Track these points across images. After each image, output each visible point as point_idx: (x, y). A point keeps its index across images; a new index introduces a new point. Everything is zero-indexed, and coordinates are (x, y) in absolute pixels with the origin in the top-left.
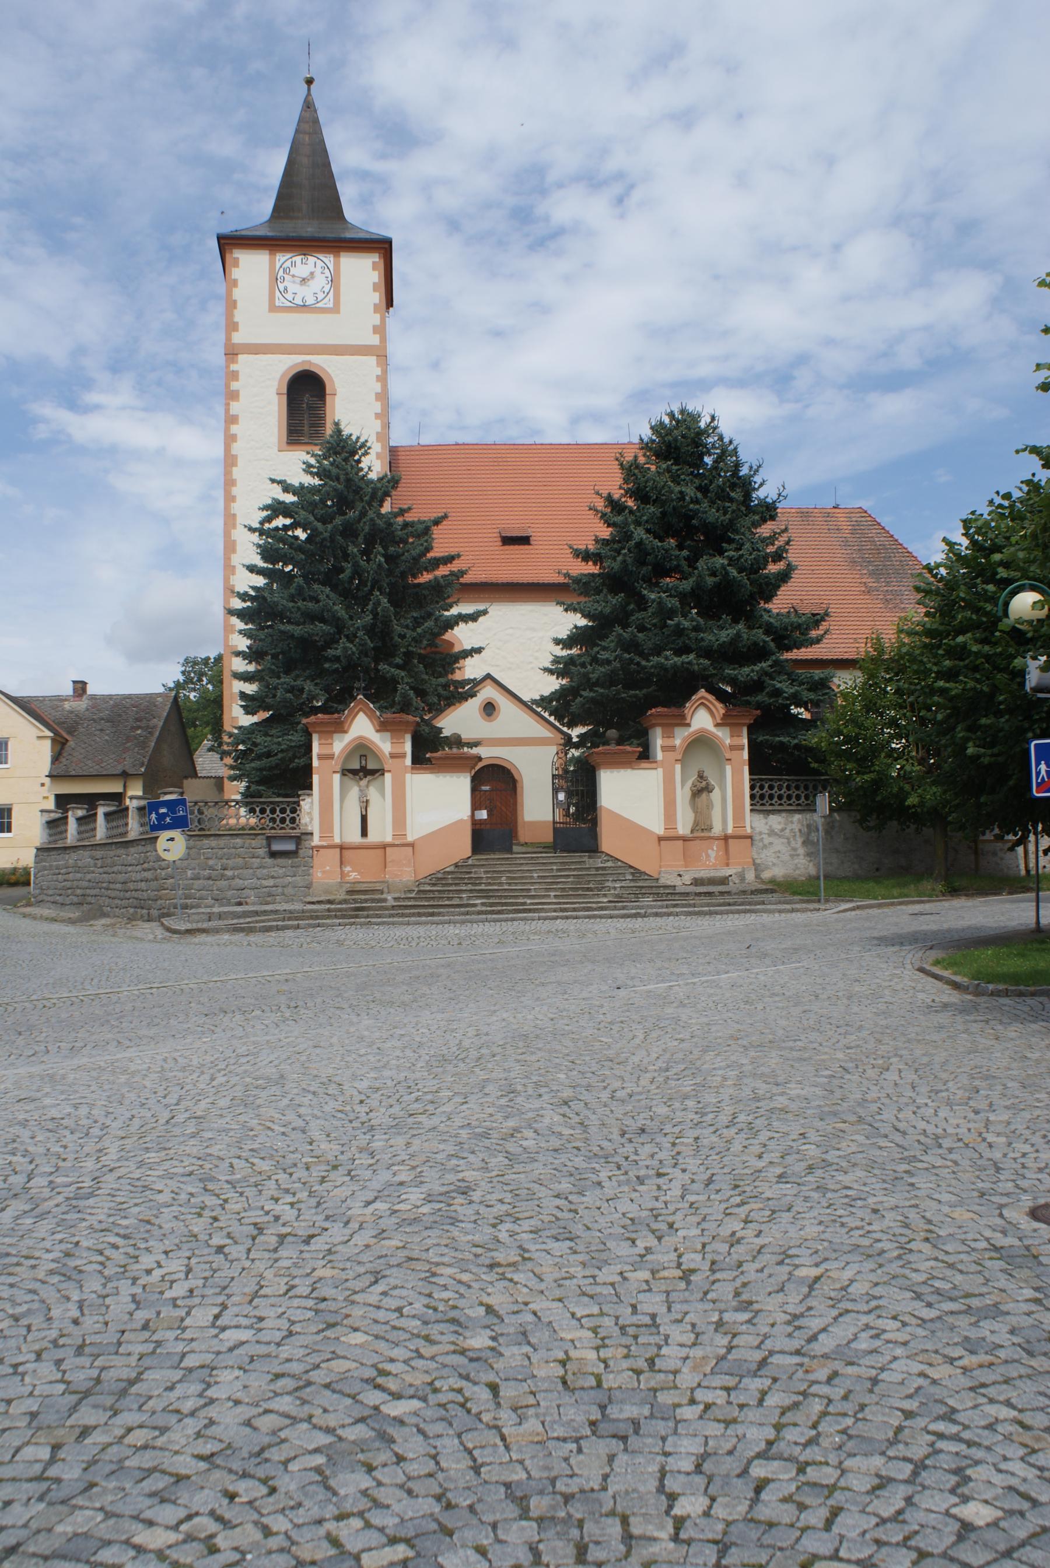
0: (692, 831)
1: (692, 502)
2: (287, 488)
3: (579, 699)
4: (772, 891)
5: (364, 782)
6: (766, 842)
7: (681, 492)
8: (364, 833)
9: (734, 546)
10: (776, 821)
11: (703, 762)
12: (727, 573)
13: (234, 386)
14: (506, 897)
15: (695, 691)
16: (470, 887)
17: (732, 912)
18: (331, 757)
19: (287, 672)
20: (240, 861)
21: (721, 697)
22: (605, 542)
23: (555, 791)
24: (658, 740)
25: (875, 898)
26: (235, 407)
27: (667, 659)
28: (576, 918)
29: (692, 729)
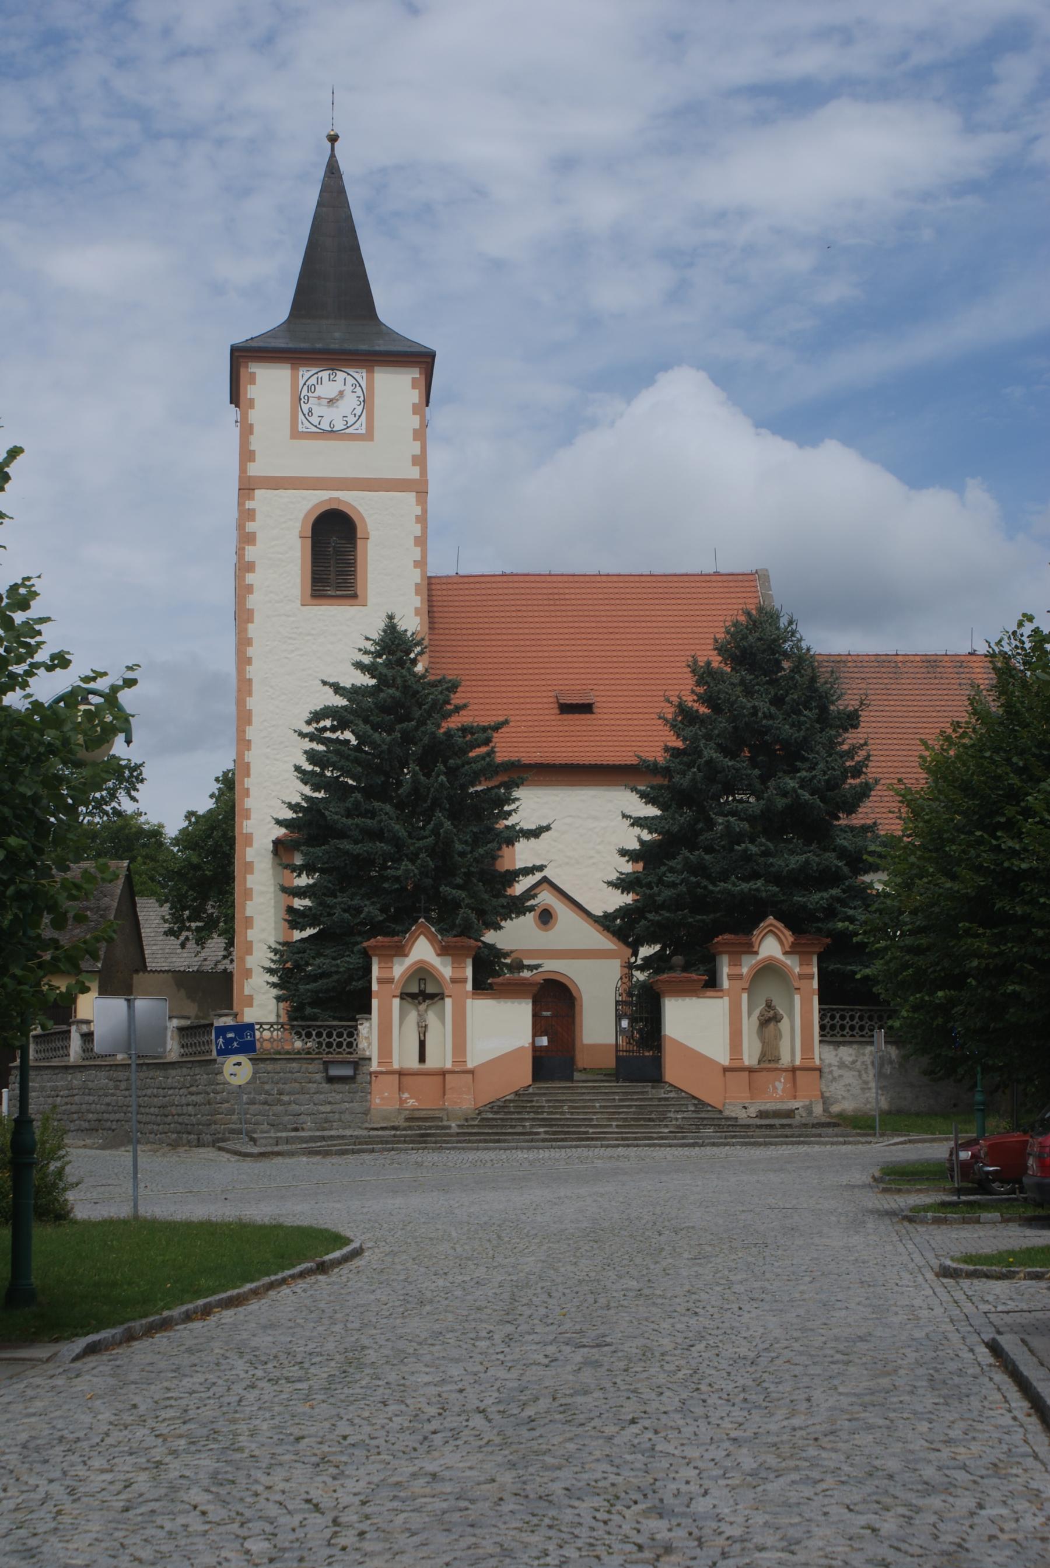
0: (759, 1062)
1: (765, 717)
2: (337, 689)
3: (643, 922)
4: (835, 1125)
5: (422, 1007)
7: (754, 707)
8: (422, 1059)
9: (807, 765)
10: (846, 1053)
11: (770, 991)
12: (798, 796)
13: (250, 527)
14: (568, 1126)
15: (763, 918)
16: (532, 1116)
17: (787, 1144)
18: (390, 981)
19: (342, 890)
22: (675, 753)
23: (619, 1018)
24: (725, 970)
25: (934, 1134)
26: (251, 553)
27: (734, 885)
28: (637, 1146)
29: (760, 957)
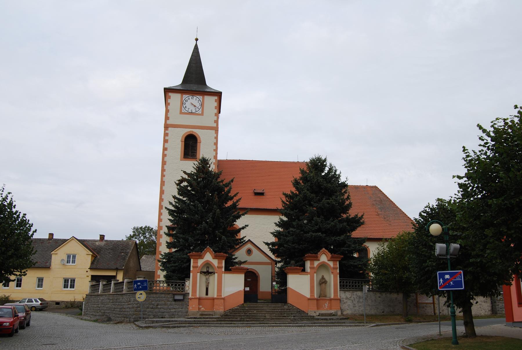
0: (319, 297)
6: (345, 301)
8: (207, 294)
10: (348, 294)
15: (321, 248)
18: (197, 267)
20: (163, 302)
21: (331, 251)
24: (308, 264)
